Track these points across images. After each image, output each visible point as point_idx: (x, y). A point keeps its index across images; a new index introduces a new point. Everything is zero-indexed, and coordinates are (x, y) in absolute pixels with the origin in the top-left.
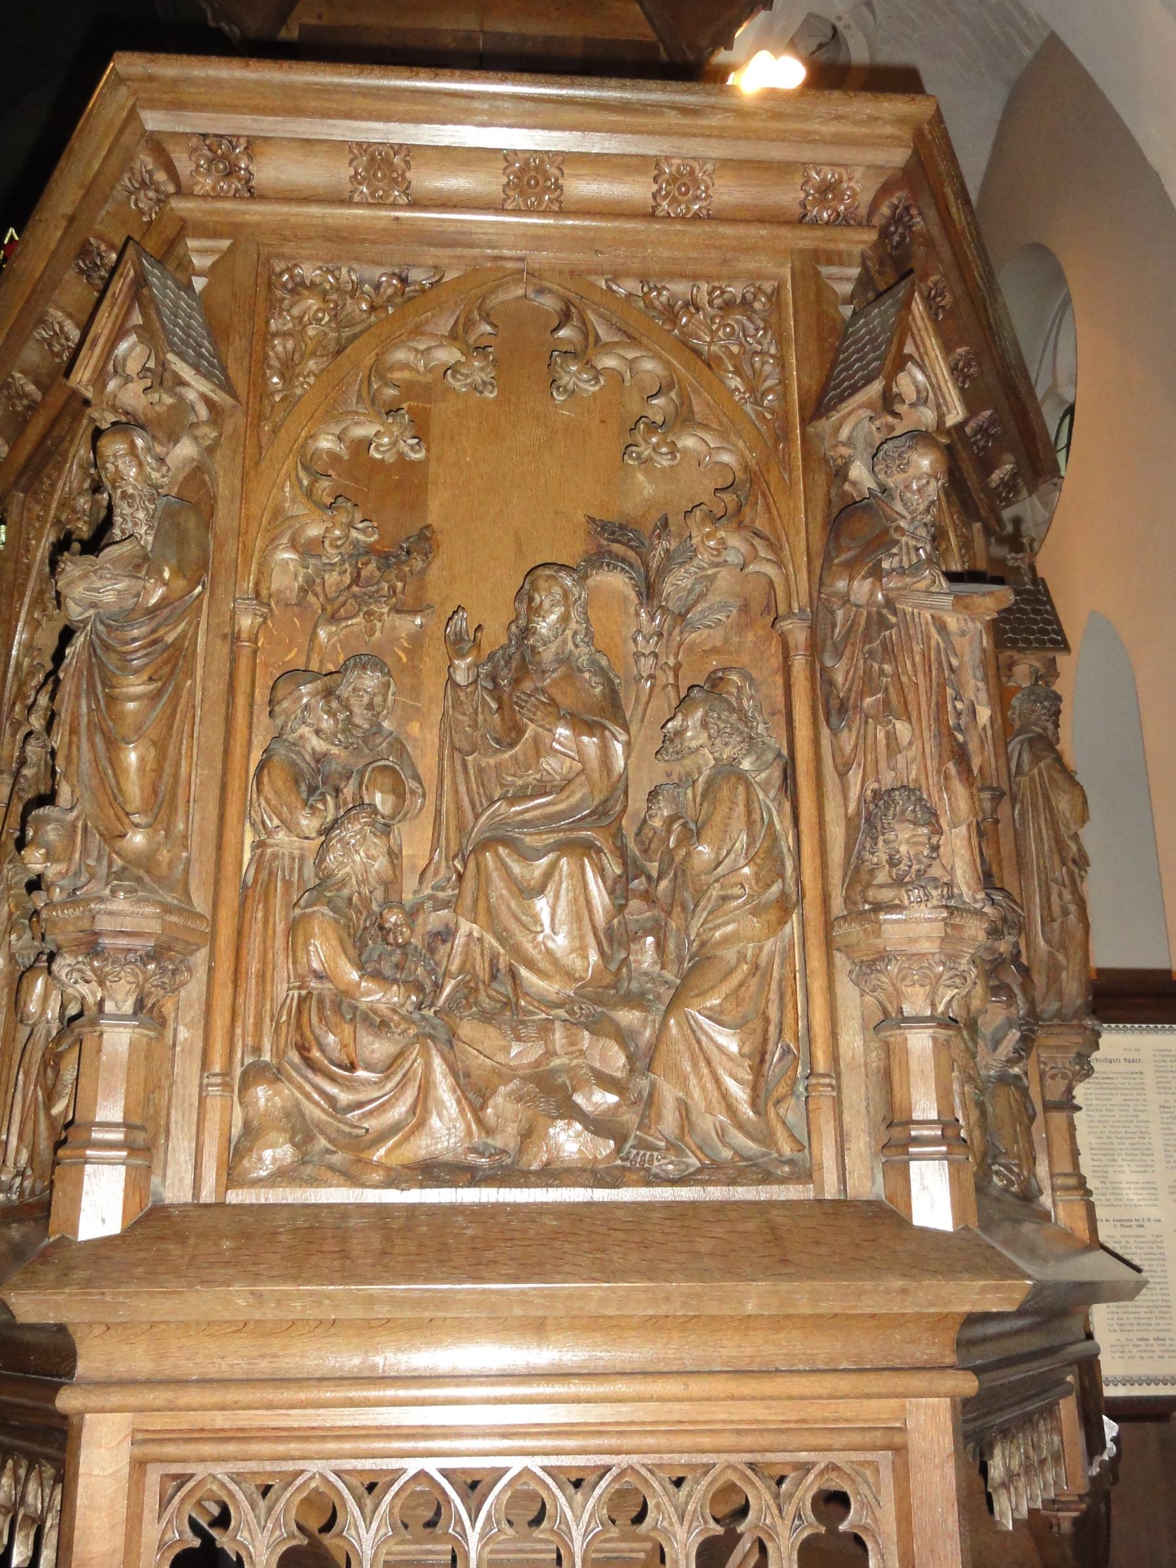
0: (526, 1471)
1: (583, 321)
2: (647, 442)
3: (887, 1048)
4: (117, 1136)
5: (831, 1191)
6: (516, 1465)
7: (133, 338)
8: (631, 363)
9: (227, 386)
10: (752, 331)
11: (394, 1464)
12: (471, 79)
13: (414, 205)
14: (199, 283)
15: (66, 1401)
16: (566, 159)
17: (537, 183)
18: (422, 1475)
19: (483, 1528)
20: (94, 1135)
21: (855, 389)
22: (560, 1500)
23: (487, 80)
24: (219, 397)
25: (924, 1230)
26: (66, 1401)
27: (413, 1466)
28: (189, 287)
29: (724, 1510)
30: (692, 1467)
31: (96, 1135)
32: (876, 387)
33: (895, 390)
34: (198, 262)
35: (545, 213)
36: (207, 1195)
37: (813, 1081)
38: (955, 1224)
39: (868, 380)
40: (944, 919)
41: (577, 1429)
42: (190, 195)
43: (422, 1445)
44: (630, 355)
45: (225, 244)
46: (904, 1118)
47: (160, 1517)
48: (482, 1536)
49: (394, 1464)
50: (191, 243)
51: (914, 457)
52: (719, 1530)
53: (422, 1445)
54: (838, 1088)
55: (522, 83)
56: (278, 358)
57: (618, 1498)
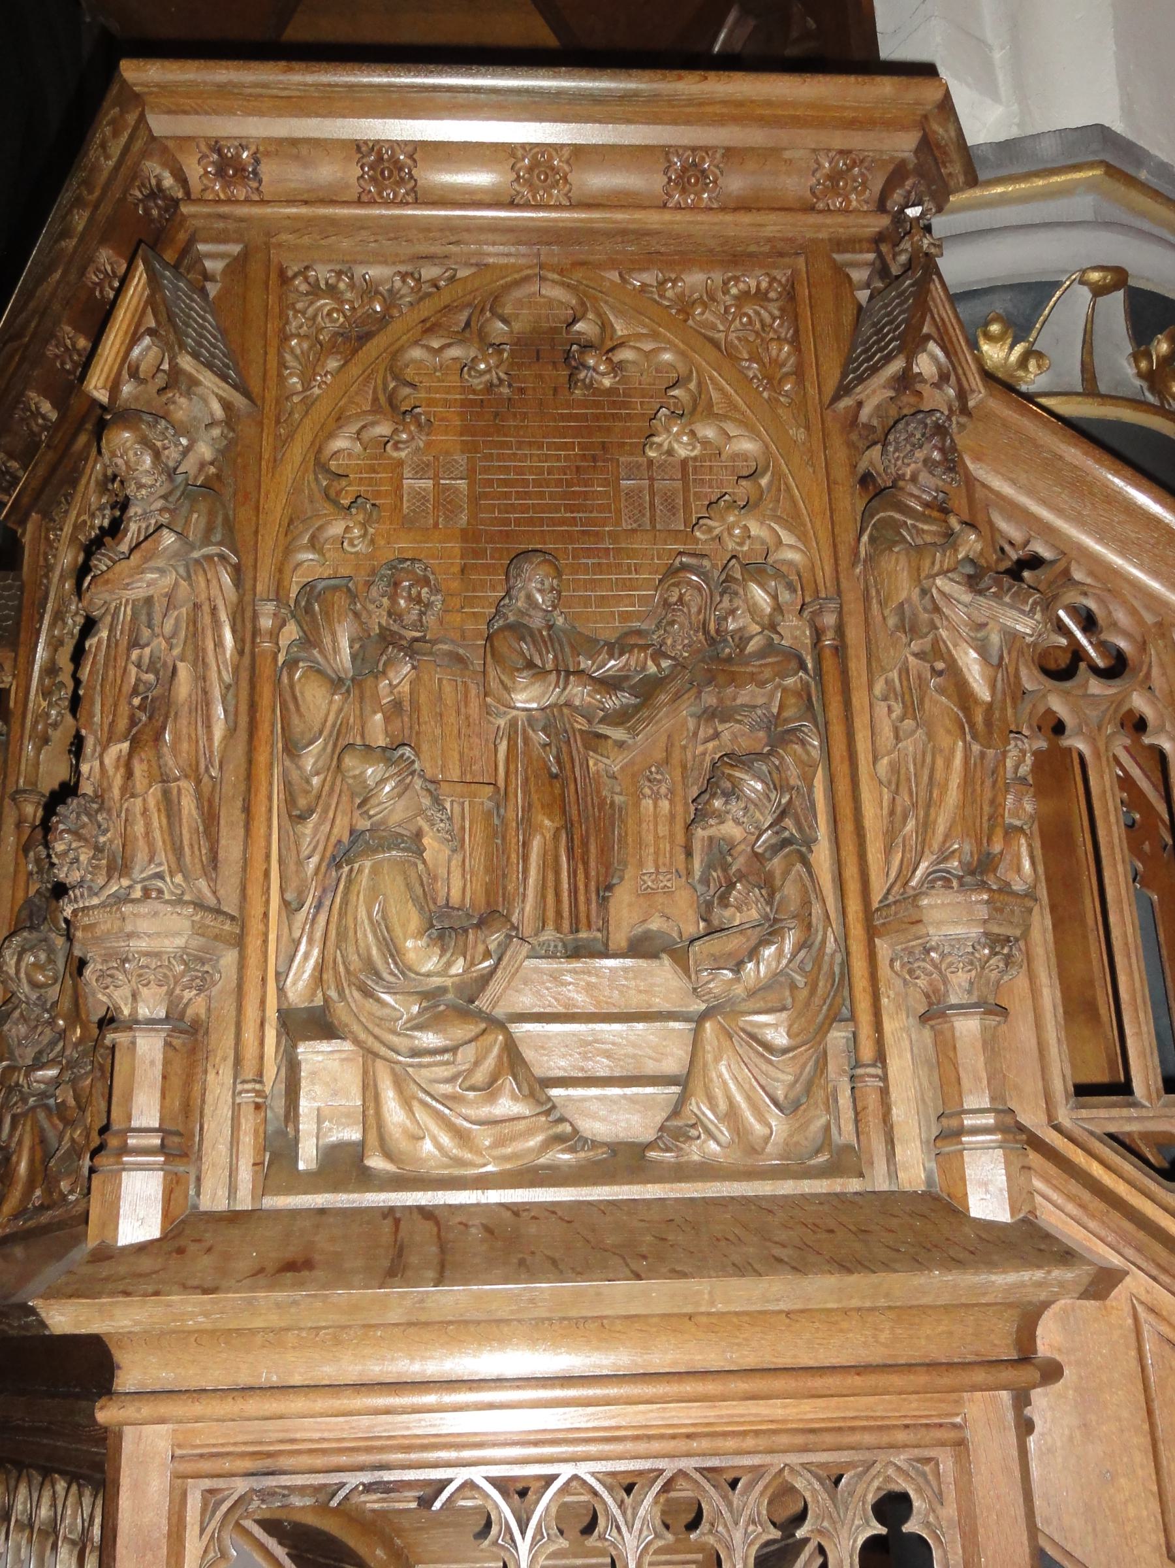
0: (575, 1477)
1: (600, 315)
2: (668, 431)
3: (937, 1034)
4: (989, 1120)
5: (882, 1184)
6: (565, 1471)
7: (147, 340)
8: (647, 355)
9: (241, 388)
10: (768, 320)
11: (334, 1479)
12: (430, 73)
13: (417, 203)
14: (213, 289)
15: (105, 1414)
16: (578, 152)
17: (382, 173)
18: (469, 1485)
19: (534, 1538)
20: (992, 1121)
21: (875, 369)
22: (712, 1500)
23: (457, 75)
24: (239, 400)
25: (975, 1219)
26: (105, 1414)
27: (461, 1475)
28: (203, 292)
29: (783, 1514)
30: (640, 1473)
31: (968, 1121)
32: (896, 366)
33: (916, 370)
34: (214, 266)
35: (558, 207)
36: (244, 1202)
37: (860, 1071)
38: (1013, 1211)
39: (888, 359)
40: (987, 902)
41: (561, 1436)
42: (200, 201)
43: (467, 1454)
44: (648, 346)
45: (235, 249)
46: (123, 1126)
47: (202, 1533)
48: (532, 1546)
49: (334, 1479)
50: (202, 247)
51: (185, 419)
52: (775, 1534)
53: (467, 1454)
54: (885, 1078)
55: (581, 78)
56: (296, 357)
57: (564, 1512)
